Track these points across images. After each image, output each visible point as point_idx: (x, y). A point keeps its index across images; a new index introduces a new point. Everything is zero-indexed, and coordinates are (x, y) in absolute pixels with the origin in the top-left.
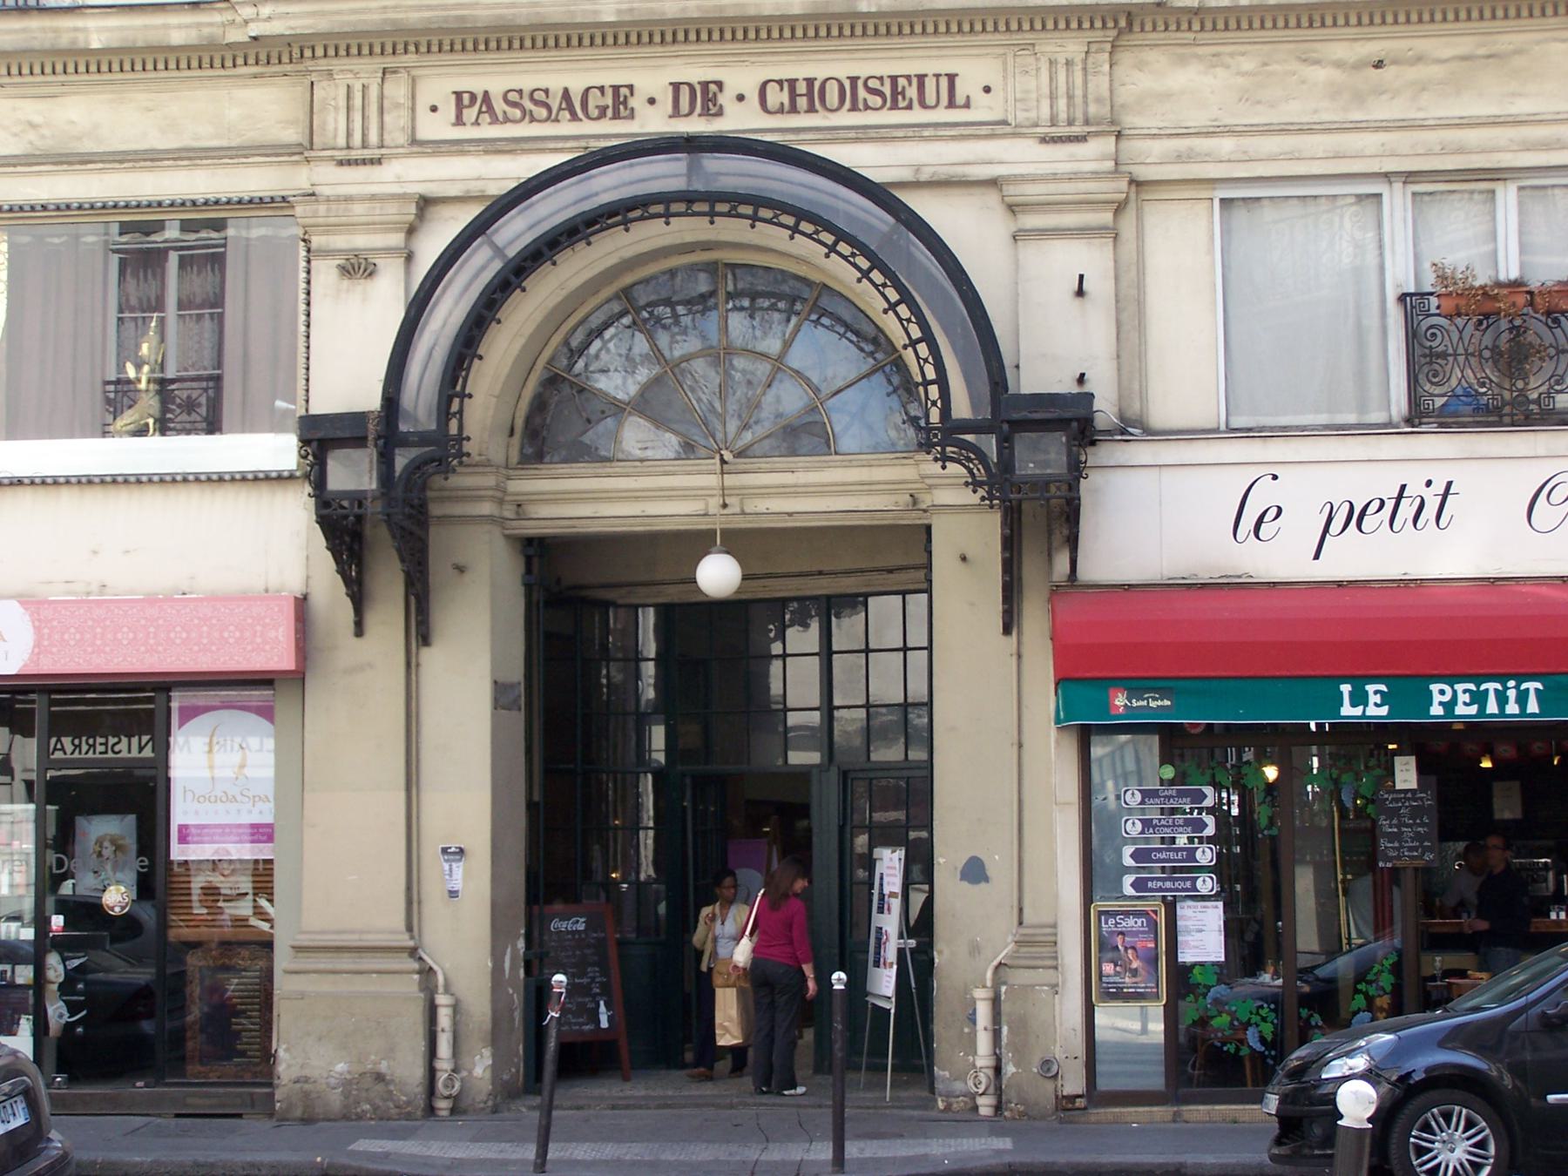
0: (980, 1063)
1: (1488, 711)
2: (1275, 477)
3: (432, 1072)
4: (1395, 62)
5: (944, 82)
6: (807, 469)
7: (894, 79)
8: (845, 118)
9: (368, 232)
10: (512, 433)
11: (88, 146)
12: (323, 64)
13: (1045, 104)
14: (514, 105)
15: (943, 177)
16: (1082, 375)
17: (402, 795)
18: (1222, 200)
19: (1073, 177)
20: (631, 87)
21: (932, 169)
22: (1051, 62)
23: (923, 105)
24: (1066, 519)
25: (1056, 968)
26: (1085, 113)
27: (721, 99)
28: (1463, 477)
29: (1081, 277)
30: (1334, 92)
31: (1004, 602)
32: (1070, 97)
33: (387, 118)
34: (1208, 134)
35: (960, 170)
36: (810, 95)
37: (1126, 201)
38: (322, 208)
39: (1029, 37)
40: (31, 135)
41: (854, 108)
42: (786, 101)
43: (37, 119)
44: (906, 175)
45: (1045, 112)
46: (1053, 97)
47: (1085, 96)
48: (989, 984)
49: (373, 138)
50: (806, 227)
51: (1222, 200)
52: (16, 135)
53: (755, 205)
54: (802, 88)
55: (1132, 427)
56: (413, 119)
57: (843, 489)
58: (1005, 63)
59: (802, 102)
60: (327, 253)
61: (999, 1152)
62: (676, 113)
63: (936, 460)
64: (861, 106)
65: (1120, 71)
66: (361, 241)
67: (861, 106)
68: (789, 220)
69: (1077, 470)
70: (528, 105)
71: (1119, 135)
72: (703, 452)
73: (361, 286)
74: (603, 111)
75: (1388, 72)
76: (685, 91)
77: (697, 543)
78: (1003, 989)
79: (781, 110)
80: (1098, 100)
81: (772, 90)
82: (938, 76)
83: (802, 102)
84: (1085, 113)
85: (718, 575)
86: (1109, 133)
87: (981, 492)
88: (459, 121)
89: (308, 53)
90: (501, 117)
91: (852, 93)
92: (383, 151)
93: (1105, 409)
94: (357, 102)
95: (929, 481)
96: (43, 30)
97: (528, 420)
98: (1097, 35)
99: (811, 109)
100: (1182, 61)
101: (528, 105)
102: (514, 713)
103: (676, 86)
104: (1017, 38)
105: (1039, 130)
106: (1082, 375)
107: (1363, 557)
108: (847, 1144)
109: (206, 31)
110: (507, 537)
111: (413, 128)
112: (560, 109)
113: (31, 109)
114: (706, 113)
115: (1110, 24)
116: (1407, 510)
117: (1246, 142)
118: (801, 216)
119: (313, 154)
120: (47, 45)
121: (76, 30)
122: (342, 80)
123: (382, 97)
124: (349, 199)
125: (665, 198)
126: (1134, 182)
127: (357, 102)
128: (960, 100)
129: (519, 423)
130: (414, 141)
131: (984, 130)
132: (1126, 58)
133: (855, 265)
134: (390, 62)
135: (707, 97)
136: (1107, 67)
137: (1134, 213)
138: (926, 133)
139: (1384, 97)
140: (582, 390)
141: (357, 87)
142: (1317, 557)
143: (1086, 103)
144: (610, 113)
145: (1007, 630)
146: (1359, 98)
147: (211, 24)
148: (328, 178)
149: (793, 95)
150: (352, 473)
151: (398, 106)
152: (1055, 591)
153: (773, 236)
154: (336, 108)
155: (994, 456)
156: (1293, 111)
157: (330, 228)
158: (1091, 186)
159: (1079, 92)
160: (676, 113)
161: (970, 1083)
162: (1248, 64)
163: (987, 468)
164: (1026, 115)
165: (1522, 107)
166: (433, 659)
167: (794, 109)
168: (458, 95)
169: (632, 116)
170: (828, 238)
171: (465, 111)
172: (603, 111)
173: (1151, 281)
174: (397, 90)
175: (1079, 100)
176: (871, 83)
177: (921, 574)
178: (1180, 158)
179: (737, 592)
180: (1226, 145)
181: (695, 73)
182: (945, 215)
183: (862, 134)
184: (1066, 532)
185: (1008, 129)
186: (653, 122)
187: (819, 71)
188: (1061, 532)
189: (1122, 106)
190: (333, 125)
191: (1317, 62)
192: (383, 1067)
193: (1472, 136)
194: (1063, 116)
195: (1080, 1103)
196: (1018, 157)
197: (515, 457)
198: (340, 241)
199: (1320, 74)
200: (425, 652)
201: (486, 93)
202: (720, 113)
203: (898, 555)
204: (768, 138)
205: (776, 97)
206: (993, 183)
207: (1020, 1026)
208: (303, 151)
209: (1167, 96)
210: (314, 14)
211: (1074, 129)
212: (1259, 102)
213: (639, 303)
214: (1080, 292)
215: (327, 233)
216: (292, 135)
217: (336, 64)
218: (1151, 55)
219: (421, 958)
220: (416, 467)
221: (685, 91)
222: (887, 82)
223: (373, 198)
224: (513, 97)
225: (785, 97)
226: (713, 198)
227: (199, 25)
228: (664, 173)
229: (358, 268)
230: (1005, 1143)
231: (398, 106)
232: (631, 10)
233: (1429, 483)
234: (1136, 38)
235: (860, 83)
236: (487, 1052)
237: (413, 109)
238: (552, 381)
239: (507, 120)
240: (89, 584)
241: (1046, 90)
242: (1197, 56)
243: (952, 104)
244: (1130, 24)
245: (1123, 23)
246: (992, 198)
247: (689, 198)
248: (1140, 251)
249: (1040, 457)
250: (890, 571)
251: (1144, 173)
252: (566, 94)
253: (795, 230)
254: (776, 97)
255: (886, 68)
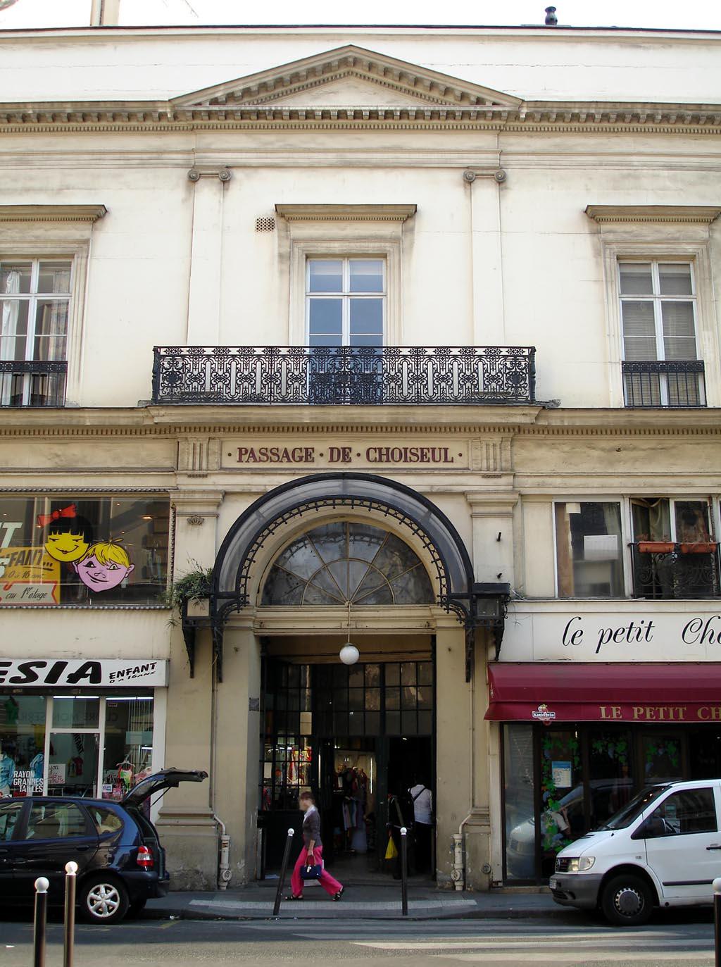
0: (456, 867)
1: (660, 718)
2: (580, 619)
3: (219, 869)
4: (625, 449)
5: (443, 451)
6: (384, 610)
7: (422, 449)
8: (401, 465)
9: (200, 506)
10: (258, 592)
11: (81, 465)
12: (184, 435)
13: (485, 461)
14: (274, 454)
15: (442, 491)
16: (501, 574)
17: (209, 747)
18: (555, 503)
19: (497, 492)
20: (313, 449)
21: (437, 487)
22: (487, 445)
23: (434, 460)
24: (496, 633)
25: (489, 825)
26: (501, 466)
27: (350, 455)
28: (655, 619)
29: (500, 533)
30: (601, 460)
31: (467, 668)
32: (495, 459)
33: (210, 458)
34: (550, 476)
35: (449, 488)
36: (387, 455)
37: (517, 503)
38: (182, 496)
39: (478, 435)
40: (57, 460)
41: (406, 461)
42: (378, 457)
43: (59, 453)
44: (427, 489)
45: (485, 465)
46: (488, 459)
47: (501, 459)
48: (460, 832)
49: (204, 466)
50: (391, 511)
51: (555, 503)
52: (49, 459)
53: (372, 501)
54: (384, 452)
55: (522, 597)
56: (221, 459)
57: (399, 619)
58: (468, 444)
59: (384, 458)
60: (183, 514)
61: (472, 906)
62: (332, 460)
63: (445, 609)
64: (408, 460)
65: (515, 448)
66: (197, 509)
67: (408, 460)
68: (385, 508)
69: (503, 615)
70: (270, 454)
71: (514, 475)
72: (185, 351)
73: (196, 528)
74: (301, 459)
75: (622, 454)
76: (335, 452)
77: (340, 641)
78: (467, 835)
79: (375, 460)
80: (506, 461)
81: (372, 452)
82: (440, 449)
83: (384, 458)
84: (501, 466)
85: (349, 654)
86: (511, 474)
87: (463, 624)
88: (240, 460)
89: (178, 430)
90: (258, 460)
91: (405, 455)
92: (209, 472)
93: (512, 592)
94: (198, 451)
95: (435, 617)
96: (66, 417)
97: (266, 586)
98: (506, 435)
99: (388, 461)
100: (539, 446)
101: (270, 454)
102: (256, 712)
103: (332, 449)
104: (474, 435)
105: (482, 472)
106: (501, 574)
107: (614, 653)
108: (408, 903)
109: (136, 420)
110: (255, 636)
111: (221, 463)
112: (283, 457)
113: (57, 449)
114: (344, 460)
115: (512, 430)
116: (634, 633)
117: (567, 480)
118: (389, 507)
119: (178, 472)
120: (67, 423)
121: (80, 417)
122: (191, 442)
123: (208, 449)
124: (193, 492)
125: (333, 498)
126: (521, 495)
127: (198, 451)
128: (449, 459)
129: (262, 588)
130: (221, 468)
131: (459, 472)
132: (517, 444)
133: (328, 505)
134: (212, 435)
135: (345, 455)
136: (509, 447)
137: (520, 507)
138: (436, 472)
139: (621, 463)
140: (289, 574)
141: (198, 444)
142: (597, 652)
143: (501, 461)
144: (304, 459)
145: (468, 680)
146: (611, 463)
147: (138, 417)
148: (184, 482)
149: (380, 455)
150: (200, 610)
151: (215, 453)
152: (489, 664)
153: (377, 515)
154: (188, 454)
155: (469, 609)
156: (585, 468)
157: (184, 503)
158: (504, 496)
159: (498, 457)
160: (332, 460)
161: (452, 876)
162: (566, 448)
163: (466, 614)
164: (476, 466)
165: (675, 469)
166: (223, 688)
167: (381, 460)
168: (240, 449)
169: (313, 461)
170: (401, 516)
171: (243, 456)
172: (301, 459)
173: (526, 534)
174: (214, 446)
175: (498, 461)
176: (412, 451)
177: (429, 654)
178: (539, 486)
179: (359, 660)
180: (558, 481)
181: (340, 444)
182: (447, 507)
183: (409, 472)
184: (494, 639)
185: (469, 472)
186: (322, 464)
187: (392, 445)
188: (491, 640)
189: (516, 463)
190: (187, 461)
191: (594, 448)
192: (198, 868)
193: (657, 481)
194: (492, 467)
195: (500, 884)
196: (473, 483)
197: (260, 601)
198: (189, 509)
199: (595, 453)
200: (220, 685)
201: (252, 449)
202: (350, 461)
203: (421, 650)
204: (370, 472)
205: (373, 455)
206: (463, 494)
207: (475, 851)
208: (173, 471)
209: (533, 460)
210: (181, 414)
211: (496, 472)
212: (571, 464)
213: (312, 537)
214: (499, 540)
215: (183, 505)
216: (168, 464)
217: (189, 435)
218: (528, 443)
219: (215, 819)
220: (223, 608)
221: (335, 452)
222: (419, 451)
223: (204, 492)
224: (263, 451)
225: (377, 455)
226: (353, 498)
227: (133, 417)
228: (333, 487)
229: (195, 521)
230: (473, 902)
231: (215, 453)
232: (316, 418)
233: (643, 622)
234: (522, 436)
235: (408, 451)
236: (243, 861)
237: (221, 455)
238: (275, 569)
239: (260, 461)
240: (74, 652)
241: (485, 456)
242: (545, 444)
243: (446, 461)
244: (519, 431)
245: (517, 430)
246: (462, 500)
247: (343, 498)
248: (523, 523)
249: (486, 612)
250: (411, 652)
251: (525, 491)
252: (286, 451)
253: (387, 512)
254: (373, 455)
255: (419, 445)
